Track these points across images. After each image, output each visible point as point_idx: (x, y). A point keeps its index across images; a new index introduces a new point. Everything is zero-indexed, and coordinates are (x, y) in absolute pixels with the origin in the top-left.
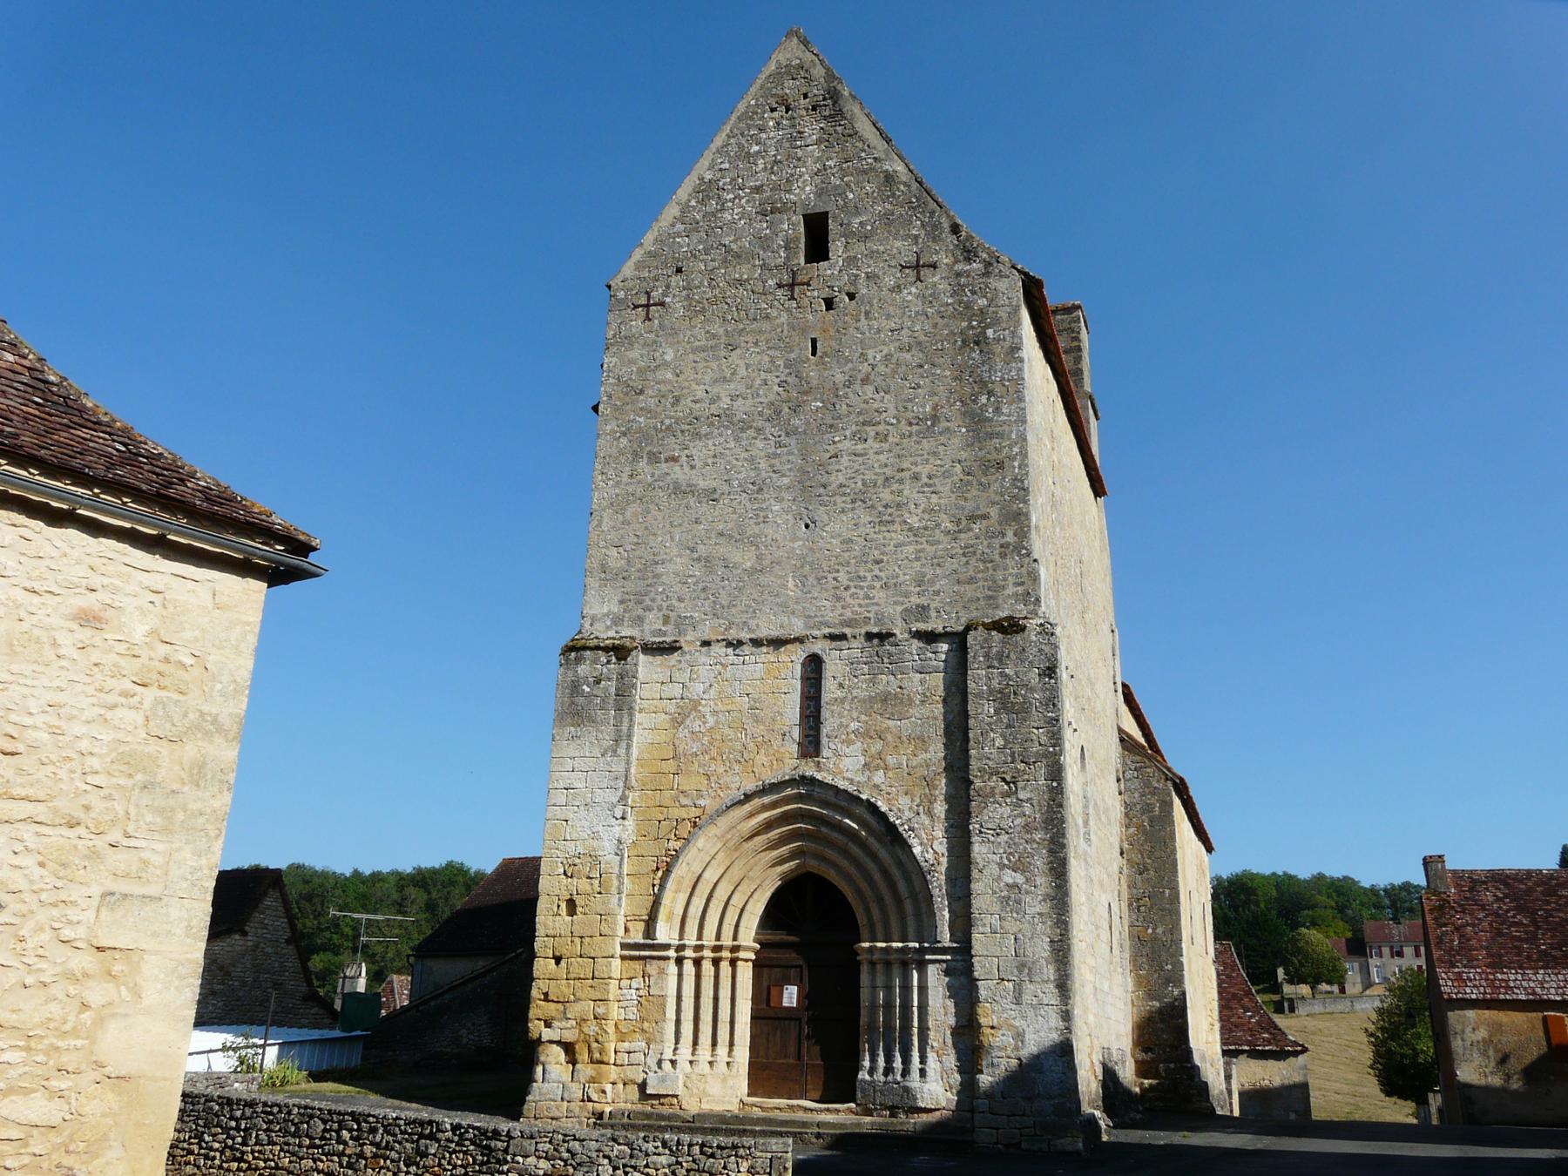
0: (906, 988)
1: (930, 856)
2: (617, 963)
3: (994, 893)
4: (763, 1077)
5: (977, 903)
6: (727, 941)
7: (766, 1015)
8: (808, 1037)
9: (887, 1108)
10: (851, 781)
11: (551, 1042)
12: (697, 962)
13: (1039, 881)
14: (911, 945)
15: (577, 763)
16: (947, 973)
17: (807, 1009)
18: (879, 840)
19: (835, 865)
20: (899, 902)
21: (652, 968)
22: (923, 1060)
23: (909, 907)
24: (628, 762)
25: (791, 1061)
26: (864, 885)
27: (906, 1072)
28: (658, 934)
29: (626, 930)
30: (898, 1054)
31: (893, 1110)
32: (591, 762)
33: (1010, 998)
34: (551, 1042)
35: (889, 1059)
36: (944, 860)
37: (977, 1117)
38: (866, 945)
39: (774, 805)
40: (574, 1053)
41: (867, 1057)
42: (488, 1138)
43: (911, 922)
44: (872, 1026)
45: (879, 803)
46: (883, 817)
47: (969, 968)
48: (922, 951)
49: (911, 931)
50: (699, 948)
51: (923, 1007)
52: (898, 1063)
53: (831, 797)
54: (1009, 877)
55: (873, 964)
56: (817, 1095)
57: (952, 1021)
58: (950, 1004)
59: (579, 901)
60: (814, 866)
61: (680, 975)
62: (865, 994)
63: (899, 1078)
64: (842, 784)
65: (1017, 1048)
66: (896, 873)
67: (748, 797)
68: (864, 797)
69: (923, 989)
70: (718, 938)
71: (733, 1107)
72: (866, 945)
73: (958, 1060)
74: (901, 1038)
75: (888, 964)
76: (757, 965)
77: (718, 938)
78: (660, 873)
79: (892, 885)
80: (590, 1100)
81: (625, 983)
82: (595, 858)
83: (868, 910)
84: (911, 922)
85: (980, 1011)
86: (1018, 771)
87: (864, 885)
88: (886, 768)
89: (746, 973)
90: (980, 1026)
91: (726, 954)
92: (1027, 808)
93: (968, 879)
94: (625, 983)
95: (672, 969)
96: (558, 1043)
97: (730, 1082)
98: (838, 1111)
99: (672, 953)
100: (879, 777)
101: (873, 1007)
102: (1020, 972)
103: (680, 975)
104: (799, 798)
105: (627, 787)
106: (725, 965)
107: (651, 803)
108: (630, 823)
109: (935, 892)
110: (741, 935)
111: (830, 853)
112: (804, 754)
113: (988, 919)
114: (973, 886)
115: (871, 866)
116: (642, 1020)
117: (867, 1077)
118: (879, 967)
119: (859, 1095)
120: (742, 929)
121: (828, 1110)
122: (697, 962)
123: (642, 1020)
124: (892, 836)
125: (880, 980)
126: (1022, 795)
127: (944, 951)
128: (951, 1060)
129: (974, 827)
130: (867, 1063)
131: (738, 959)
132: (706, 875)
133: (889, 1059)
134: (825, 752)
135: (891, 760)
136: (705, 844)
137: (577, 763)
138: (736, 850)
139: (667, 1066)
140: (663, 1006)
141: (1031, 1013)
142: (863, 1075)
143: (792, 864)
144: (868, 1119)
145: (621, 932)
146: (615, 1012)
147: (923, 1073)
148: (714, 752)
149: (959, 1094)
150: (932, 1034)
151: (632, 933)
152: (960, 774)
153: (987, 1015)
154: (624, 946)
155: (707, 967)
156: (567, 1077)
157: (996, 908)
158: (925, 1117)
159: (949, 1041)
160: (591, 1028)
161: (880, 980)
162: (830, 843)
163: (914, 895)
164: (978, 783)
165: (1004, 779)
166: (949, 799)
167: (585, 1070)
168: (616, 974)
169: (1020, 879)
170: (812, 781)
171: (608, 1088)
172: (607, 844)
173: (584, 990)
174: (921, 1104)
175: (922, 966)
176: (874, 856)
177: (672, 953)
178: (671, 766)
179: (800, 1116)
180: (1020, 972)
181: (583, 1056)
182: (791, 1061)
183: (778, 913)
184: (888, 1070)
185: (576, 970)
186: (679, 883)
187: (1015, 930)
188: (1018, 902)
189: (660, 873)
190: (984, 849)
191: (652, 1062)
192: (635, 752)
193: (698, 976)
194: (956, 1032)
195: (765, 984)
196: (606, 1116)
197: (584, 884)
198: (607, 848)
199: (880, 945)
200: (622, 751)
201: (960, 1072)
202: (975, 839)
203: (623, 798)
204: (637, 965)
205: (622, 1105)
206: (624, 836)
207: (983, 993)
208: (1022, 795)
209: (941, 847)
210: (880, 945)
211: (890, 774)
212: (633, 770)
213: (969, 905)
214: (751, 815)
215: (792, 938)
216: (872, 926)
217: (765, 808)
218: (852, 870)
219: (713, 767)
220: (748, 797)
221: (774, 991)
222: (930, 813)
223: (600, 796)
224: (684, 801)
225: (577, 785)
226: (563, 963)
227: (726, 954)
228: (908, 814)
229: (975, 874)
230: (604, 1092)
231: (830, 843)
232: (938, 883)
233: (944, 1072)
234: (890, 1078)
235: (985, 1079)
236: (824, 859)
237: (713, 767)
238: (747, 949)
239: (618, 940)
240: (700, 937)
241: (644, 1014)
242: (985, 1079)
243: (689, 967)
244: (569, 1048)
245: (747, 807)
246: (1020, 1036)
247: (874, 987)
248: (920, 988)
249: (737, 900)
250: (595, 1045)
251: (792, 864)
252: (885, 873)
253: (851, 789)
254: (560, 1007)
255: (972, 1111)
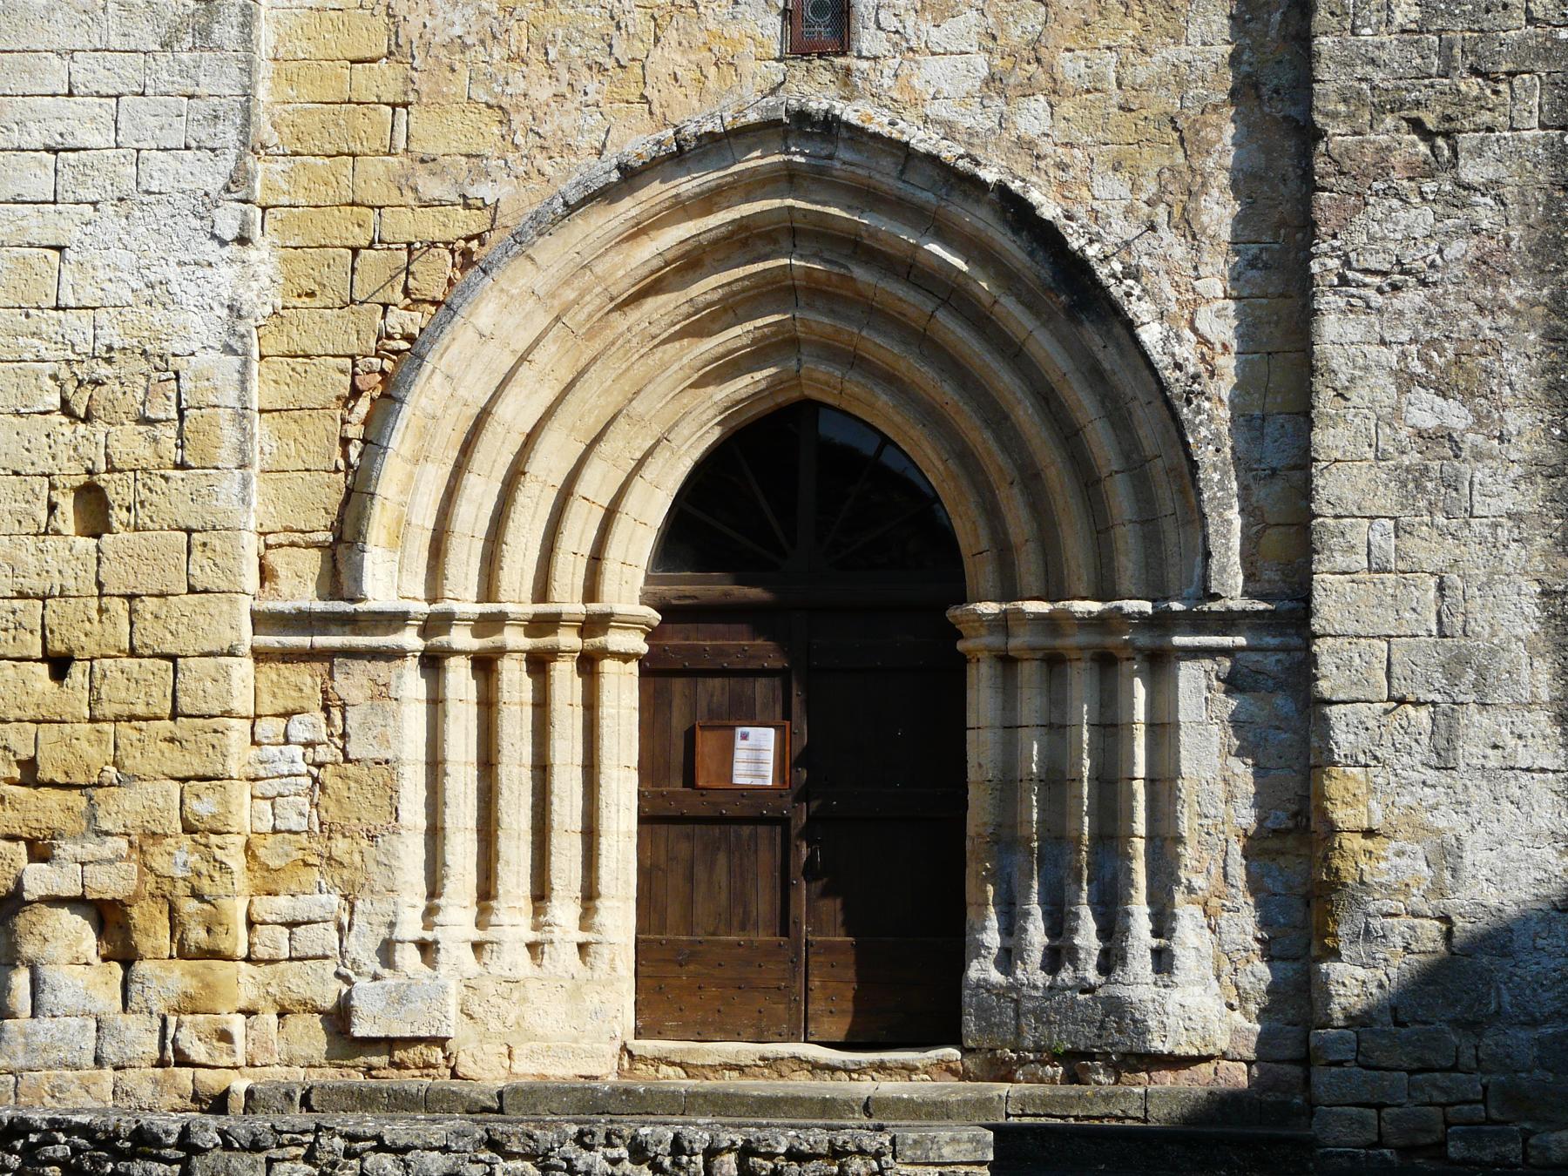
0: (1111, 729)
1: (1187, 350)
2: (243, 667)
3: (1381, 456)
4: (674, 981)
5: (1330, 486)
6: (568, 599)
7: (682, 809)
8: (810, 872)
9: (1056, 1058)
10: (949, 130)
11: (55, 901)
12: (485, 665)
13: (1516, 420)
14: (1131, 606)
15: (86, 71)
16: (1232, 684)
17: (803, 795)
18: (1031, 304)
19: (890, 380)
20: (1089, 482)
21: (353, 682)
22: (1163, 923)
23: (1120, 498)
24: (248, 68)
25: (763, 937)
26: (980, 438)
27: (1111, 960)
28: (368, 586)
29: (266, 574)
30: (1086, 912)
31: (1075, 1064)
32: (129, 71)
33: (1422, 751)
34: (55, 901)
35: (1060, 924)
36: (1228, 364)
37: (1322, 1077)
38: (990, 608)
39: (708, 201)
40: (125, 928)
41: (993, 922)
42: (119, 1155)
43: (1127, 540)
44: (1006, 839)
45: (1035, 197)
46: (1045, 236)
47: (1304, 668)
48: (1162, 622)
49: (1128, 564)
50: (489, 623)
51: (1163, 782)
52: (1087, 936)
53: (885, 176)
54: (1426, 410)
55: (1007, 662)
56: (838, 1028)
57: (1247, 818)
58: (1243, 772)
59: (117, 490)
60: (823, 380)
61: (436, 702)
62: (981, 751)
63: (1092, 975)
64: (923, 139)
65: (1438, 890)
66: (1083, 403)
67: (631, 177)
68: (989, 175)
69: (1163, 730)
70: (542, 591)
71: (605, 1068)
72: (990, 608)
73: (1263, 923)
74: (1099, 862)
75: (1054, 662)
76: (653, 671)
77: (542, 591)
78: (363, 406)
79: (1069, 436)
80: (183, 1061)
81: (270, 728)
82: (166, 369)
83: (993, 513)
84: (1127, 540)
85: (1333, 788)
86: (1460, 98)
87: (980, 438)
88: (1055, 90)
89: (621, 690)
90: (1332, 829)
91: (568, 639)
92: (1485, 212)
93: (1303, 416)
94: (270, 728)
95: (411, 683)
96: (77, 903)
97: (592, 1000)
98: (909, 1070)
99: (410, 639)
100: (1032, 118)
101: (1008, 785)
102: (1453, 679)
103: (436, 702)
104: (788, 179)
105: (250, 145)
106: (565, 675)
107: (323, 194)
108: (261, 254)
109: (1205, 455)
110: (451, 587)
111: (881, 346)
112: (800, 48)
113: (1359, 532)
114: (1318, 436)
115: (1005, 382)
116: (328, 830)
117: (996, 976)
118: (1029, 673)
119: (970, 1024)
120: (611, 567)
121: (881, 1067)
122: (485, 665)
123: (328, 830)
124: (1076, 290)
125: (1031, 706)
126: (1471, 171)
127: (1228, 622)
128: (1244, 925)
129: (1324, 266)
130: (992, 938)
131: (605, 653)
132: (503, 410)
133: (1060, 924)
134: (868, 40)
135: (1070, 67)
136: (498, 316)
137: (86, 71)
138: (591, 334)
139: (408, 957)
140: (392, 792)
141: (1480, 794)
142: (982, 971)
143: (762, 376)
144: (1005, 1088)
145: (251, 580)
146: (244, 812)
147: (1163, 961)
148: (518, 38)
149: (1264, 1014)
150: (1188, 854)
151: (285, 583)
152: (1279, 109)
153: (1352, 800)
154: (260, 621)
155: (514, 679)
156: (107, 998)
157: (1386, 500)
158: (1166, 1079)
159: (1238, 871)
160: (177, 858)
161: (1031, 706)
162: (875, 313)
163: (1136, 466)
164: (1338, 136)
165: (1417, 126)
166: (1244, 183)
167: (164, 978)
168: (243, 704)
169: (1456, 415)
170: (830, 127)
171: (237, 1024)
172: (196, 320)
173: (149, 750)
174: (1158, 1045)
175: (1159, 664)
176: (1013, 352)
177: (410, 639)
178: (384, 80)
179: (801, 1084)
180: (1453, 679)
181: (153, 933)
182: (763, 937)
183: (700, 526)
184: (1059, 955)
185: (119, 693)
186: (424, 433)
187: (1438, 560)
188: (1451, 484)
189: (363, 406)
190: (1353, 329)
191: (363, 947)
192: (266, 36)
193: (488, 706)
194: (1258, 847)
195: (678, 723)
196: (237, 1102)
197: (130, 443)
198: (194, 330)
199: (1081, 607)
200: (226, 32)
201: (1269, 956)
202: (1328, 301)
203: (238, 181)
204: (306, 677)
205: (278, 1073)
206: (248, 297)
207: (1343, 739)
208: (1471, 171)
209: (1220, 323)
210: (1081, 607)
211: (1067, 107)
212: (262, 93)
213: (1306, 491)
214: (640, 230)
215: (754, 593)
216: (1004, 552)
217: (681, 209)
218: (945, 392)
219: (518, 85)
220: (631, 177)
221: (706, 743)
222: (1188, 226)
223: (163, 171)
224: (432, 188)
225: (85, 137)
226: (77, 672)
227: (568, 639)
228: (1121, 228)
229: (1325, 401)
230: (225, 1036)
231: (875, 313)
232: (1212, 429)
233: (1224, 963)
234: (1066, 975)
235: (1352, 982)
236: (855, 360)
237: (518, 85)
238: (628, 623)
239: (246, 604)
240: (488, 591)
241: (333, 814)
242: (1352, 982)
243: (460, 679)
244: (108, 917)
245: (628, 208)
246: (1447, 856)
247: (1010, 728)
248: (1153, 727)
249: (597, 484)
250: (189, 906)
251: (762, 376)
252: (1048, 399)
253: (949, 151)
254: (76, 799)
255: (1305, 1061)
